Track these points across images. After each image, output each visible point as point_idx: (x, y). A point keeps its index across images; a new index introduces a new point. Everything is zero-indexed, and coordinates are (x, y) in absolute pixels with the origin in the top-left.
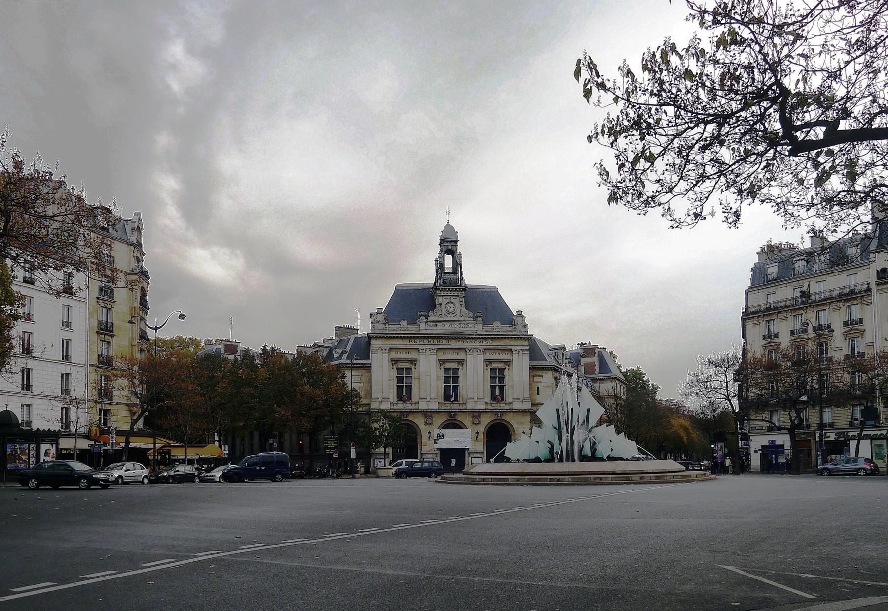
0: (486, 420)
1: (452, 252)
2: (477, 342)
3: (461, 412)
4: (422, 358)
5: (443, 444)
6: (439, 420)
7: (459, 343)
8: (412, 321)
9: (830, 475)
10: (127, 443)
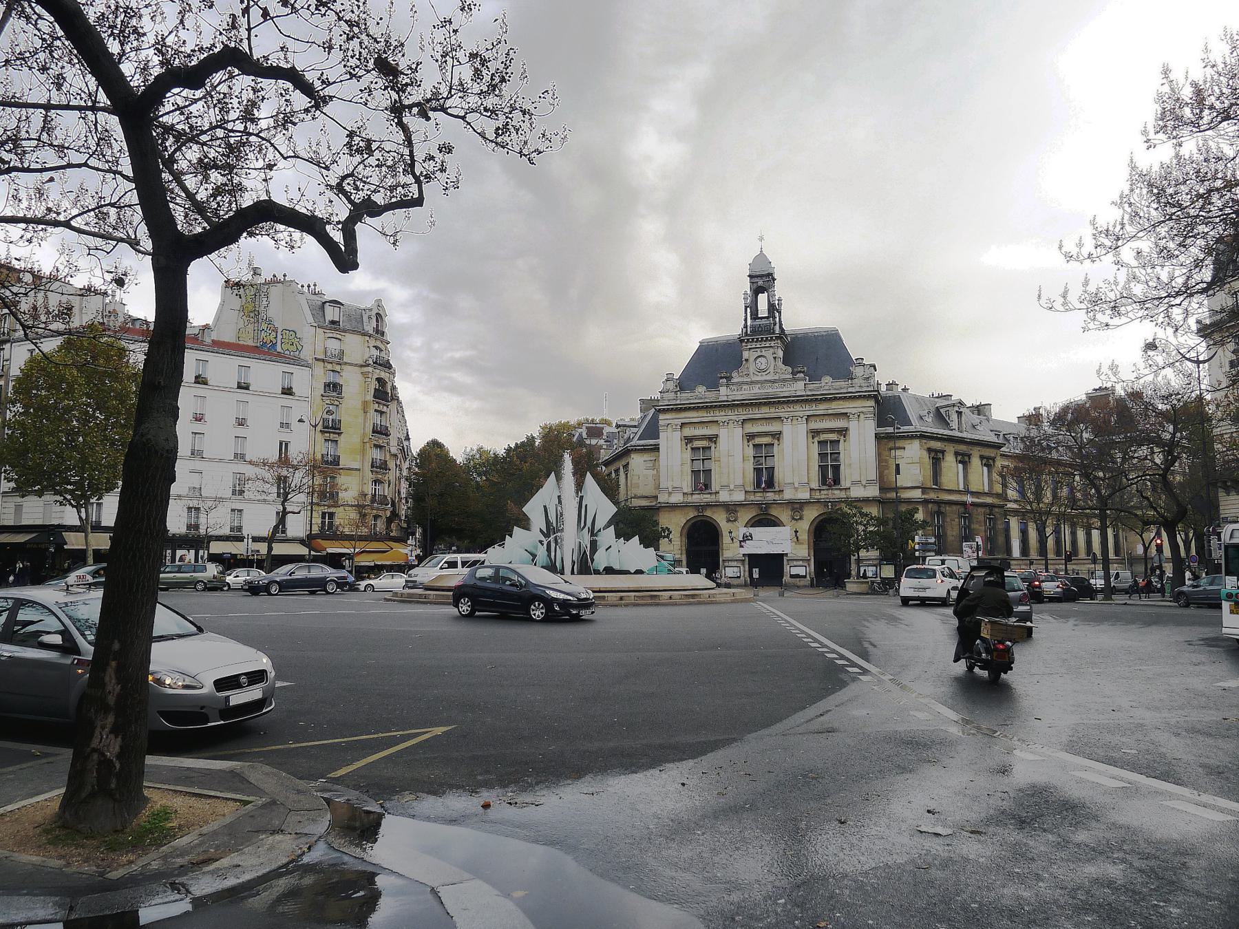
0: (811, 514)
2: (797, 407)
3: (775, 503)
4: (723, 433)
5: (752, 548)
6: (745, 516)
7: (773, 410)
8: (713, 385)
10: (270, 549)
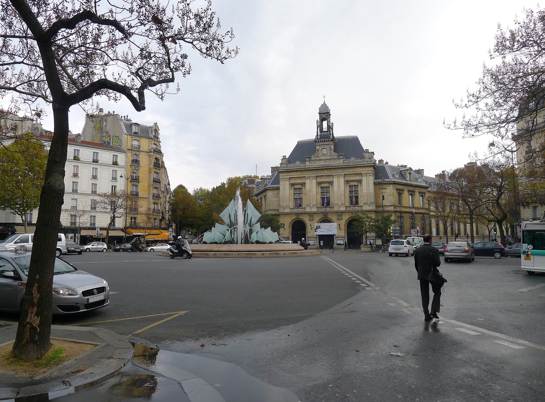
0: (346, 217)
2: (340, 171)
3: (330, 212)
5: (320, 232)
6: (317, 218)
9: (123, 251)
10: (108, 233)
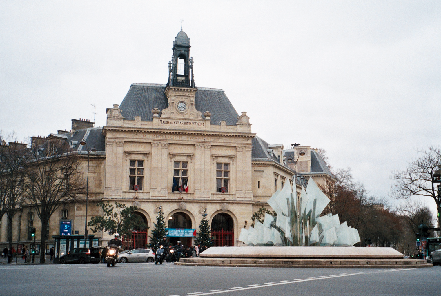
1: (182, 56)
7: (189, 139)
9: (127, 262)
